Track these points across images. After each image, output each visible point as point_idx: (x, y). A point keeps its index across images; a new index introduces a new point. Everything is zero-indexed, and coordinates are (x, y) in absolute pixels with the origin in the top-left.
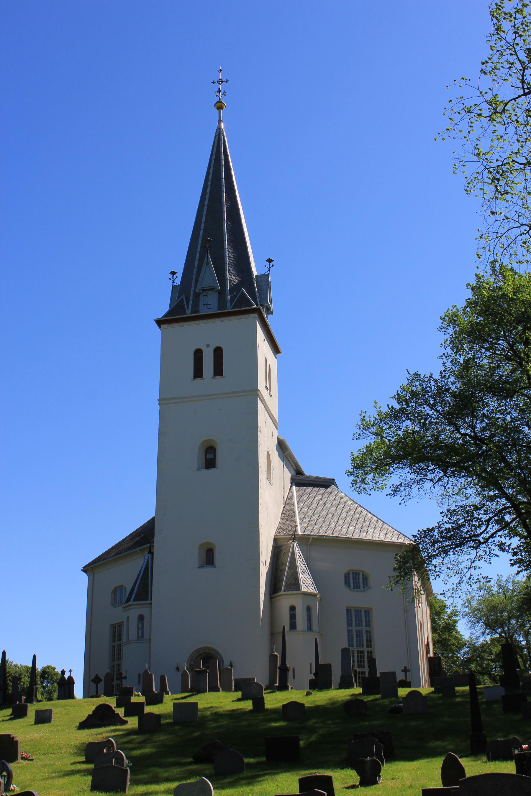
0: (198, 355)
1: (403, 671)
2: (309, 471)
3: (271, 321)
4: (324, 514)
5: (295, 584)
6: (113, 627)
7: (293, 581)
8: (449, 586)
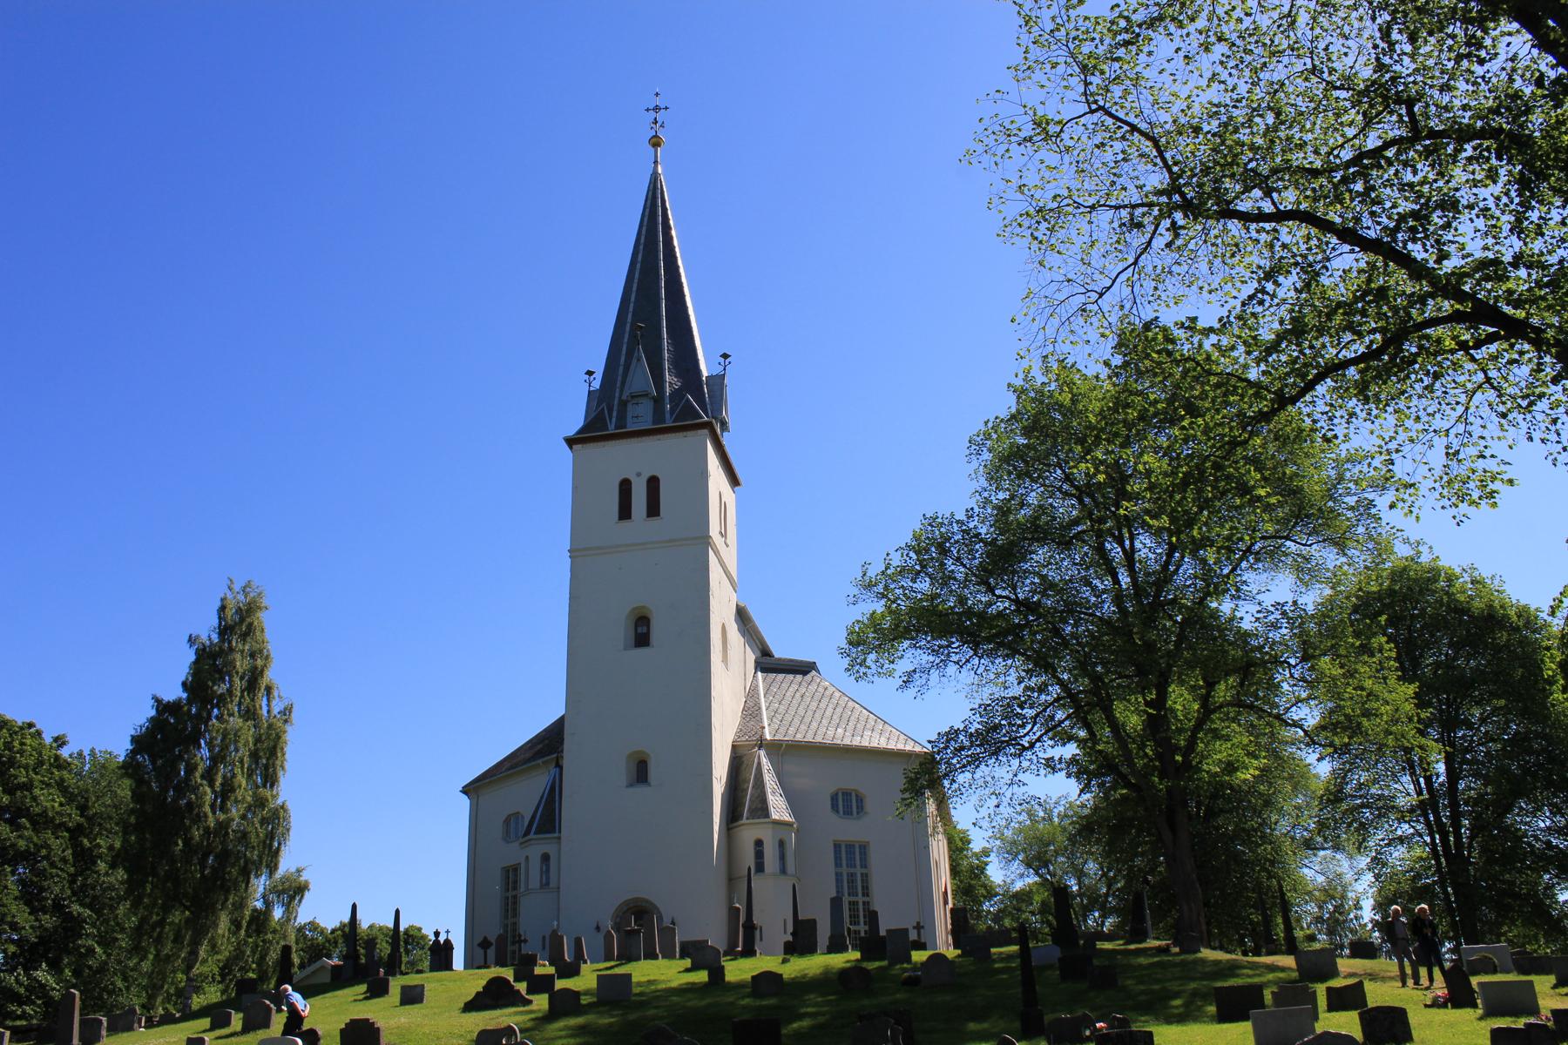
0: (625, 487)
2: (779, 652)
3: (726, 440)
4: (801, 711)
5: (762, 809)
6: (506, 870)
8: (984, 812)
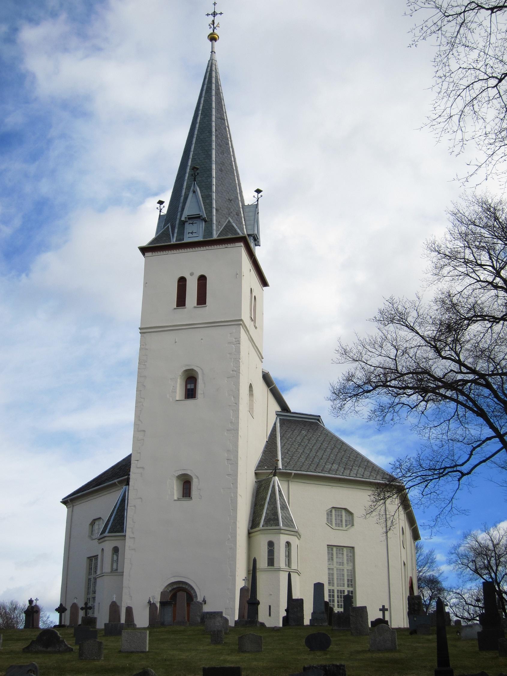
0: (182, 282)
1: (380, 610)
3: (258, 252)
7: (273, 517)
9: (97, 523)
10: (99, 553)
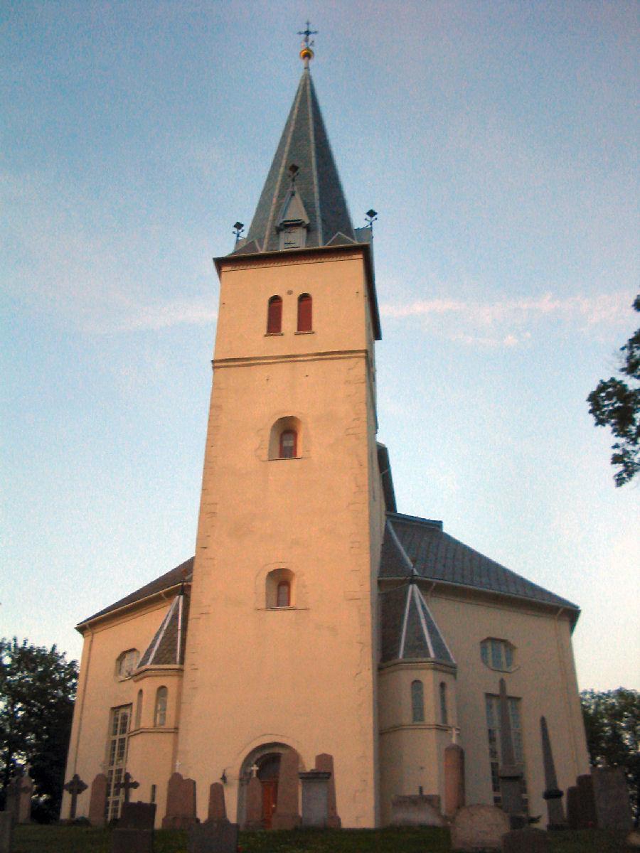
0: (275, 302)
6: (115, 709)
9: (128, 656)
10: (134, 699)
